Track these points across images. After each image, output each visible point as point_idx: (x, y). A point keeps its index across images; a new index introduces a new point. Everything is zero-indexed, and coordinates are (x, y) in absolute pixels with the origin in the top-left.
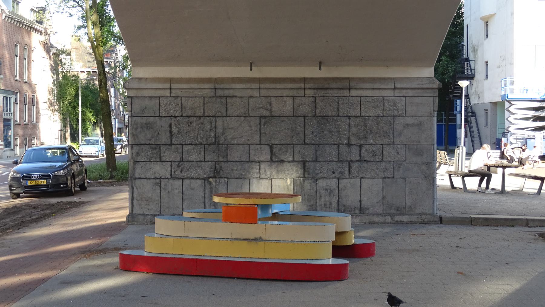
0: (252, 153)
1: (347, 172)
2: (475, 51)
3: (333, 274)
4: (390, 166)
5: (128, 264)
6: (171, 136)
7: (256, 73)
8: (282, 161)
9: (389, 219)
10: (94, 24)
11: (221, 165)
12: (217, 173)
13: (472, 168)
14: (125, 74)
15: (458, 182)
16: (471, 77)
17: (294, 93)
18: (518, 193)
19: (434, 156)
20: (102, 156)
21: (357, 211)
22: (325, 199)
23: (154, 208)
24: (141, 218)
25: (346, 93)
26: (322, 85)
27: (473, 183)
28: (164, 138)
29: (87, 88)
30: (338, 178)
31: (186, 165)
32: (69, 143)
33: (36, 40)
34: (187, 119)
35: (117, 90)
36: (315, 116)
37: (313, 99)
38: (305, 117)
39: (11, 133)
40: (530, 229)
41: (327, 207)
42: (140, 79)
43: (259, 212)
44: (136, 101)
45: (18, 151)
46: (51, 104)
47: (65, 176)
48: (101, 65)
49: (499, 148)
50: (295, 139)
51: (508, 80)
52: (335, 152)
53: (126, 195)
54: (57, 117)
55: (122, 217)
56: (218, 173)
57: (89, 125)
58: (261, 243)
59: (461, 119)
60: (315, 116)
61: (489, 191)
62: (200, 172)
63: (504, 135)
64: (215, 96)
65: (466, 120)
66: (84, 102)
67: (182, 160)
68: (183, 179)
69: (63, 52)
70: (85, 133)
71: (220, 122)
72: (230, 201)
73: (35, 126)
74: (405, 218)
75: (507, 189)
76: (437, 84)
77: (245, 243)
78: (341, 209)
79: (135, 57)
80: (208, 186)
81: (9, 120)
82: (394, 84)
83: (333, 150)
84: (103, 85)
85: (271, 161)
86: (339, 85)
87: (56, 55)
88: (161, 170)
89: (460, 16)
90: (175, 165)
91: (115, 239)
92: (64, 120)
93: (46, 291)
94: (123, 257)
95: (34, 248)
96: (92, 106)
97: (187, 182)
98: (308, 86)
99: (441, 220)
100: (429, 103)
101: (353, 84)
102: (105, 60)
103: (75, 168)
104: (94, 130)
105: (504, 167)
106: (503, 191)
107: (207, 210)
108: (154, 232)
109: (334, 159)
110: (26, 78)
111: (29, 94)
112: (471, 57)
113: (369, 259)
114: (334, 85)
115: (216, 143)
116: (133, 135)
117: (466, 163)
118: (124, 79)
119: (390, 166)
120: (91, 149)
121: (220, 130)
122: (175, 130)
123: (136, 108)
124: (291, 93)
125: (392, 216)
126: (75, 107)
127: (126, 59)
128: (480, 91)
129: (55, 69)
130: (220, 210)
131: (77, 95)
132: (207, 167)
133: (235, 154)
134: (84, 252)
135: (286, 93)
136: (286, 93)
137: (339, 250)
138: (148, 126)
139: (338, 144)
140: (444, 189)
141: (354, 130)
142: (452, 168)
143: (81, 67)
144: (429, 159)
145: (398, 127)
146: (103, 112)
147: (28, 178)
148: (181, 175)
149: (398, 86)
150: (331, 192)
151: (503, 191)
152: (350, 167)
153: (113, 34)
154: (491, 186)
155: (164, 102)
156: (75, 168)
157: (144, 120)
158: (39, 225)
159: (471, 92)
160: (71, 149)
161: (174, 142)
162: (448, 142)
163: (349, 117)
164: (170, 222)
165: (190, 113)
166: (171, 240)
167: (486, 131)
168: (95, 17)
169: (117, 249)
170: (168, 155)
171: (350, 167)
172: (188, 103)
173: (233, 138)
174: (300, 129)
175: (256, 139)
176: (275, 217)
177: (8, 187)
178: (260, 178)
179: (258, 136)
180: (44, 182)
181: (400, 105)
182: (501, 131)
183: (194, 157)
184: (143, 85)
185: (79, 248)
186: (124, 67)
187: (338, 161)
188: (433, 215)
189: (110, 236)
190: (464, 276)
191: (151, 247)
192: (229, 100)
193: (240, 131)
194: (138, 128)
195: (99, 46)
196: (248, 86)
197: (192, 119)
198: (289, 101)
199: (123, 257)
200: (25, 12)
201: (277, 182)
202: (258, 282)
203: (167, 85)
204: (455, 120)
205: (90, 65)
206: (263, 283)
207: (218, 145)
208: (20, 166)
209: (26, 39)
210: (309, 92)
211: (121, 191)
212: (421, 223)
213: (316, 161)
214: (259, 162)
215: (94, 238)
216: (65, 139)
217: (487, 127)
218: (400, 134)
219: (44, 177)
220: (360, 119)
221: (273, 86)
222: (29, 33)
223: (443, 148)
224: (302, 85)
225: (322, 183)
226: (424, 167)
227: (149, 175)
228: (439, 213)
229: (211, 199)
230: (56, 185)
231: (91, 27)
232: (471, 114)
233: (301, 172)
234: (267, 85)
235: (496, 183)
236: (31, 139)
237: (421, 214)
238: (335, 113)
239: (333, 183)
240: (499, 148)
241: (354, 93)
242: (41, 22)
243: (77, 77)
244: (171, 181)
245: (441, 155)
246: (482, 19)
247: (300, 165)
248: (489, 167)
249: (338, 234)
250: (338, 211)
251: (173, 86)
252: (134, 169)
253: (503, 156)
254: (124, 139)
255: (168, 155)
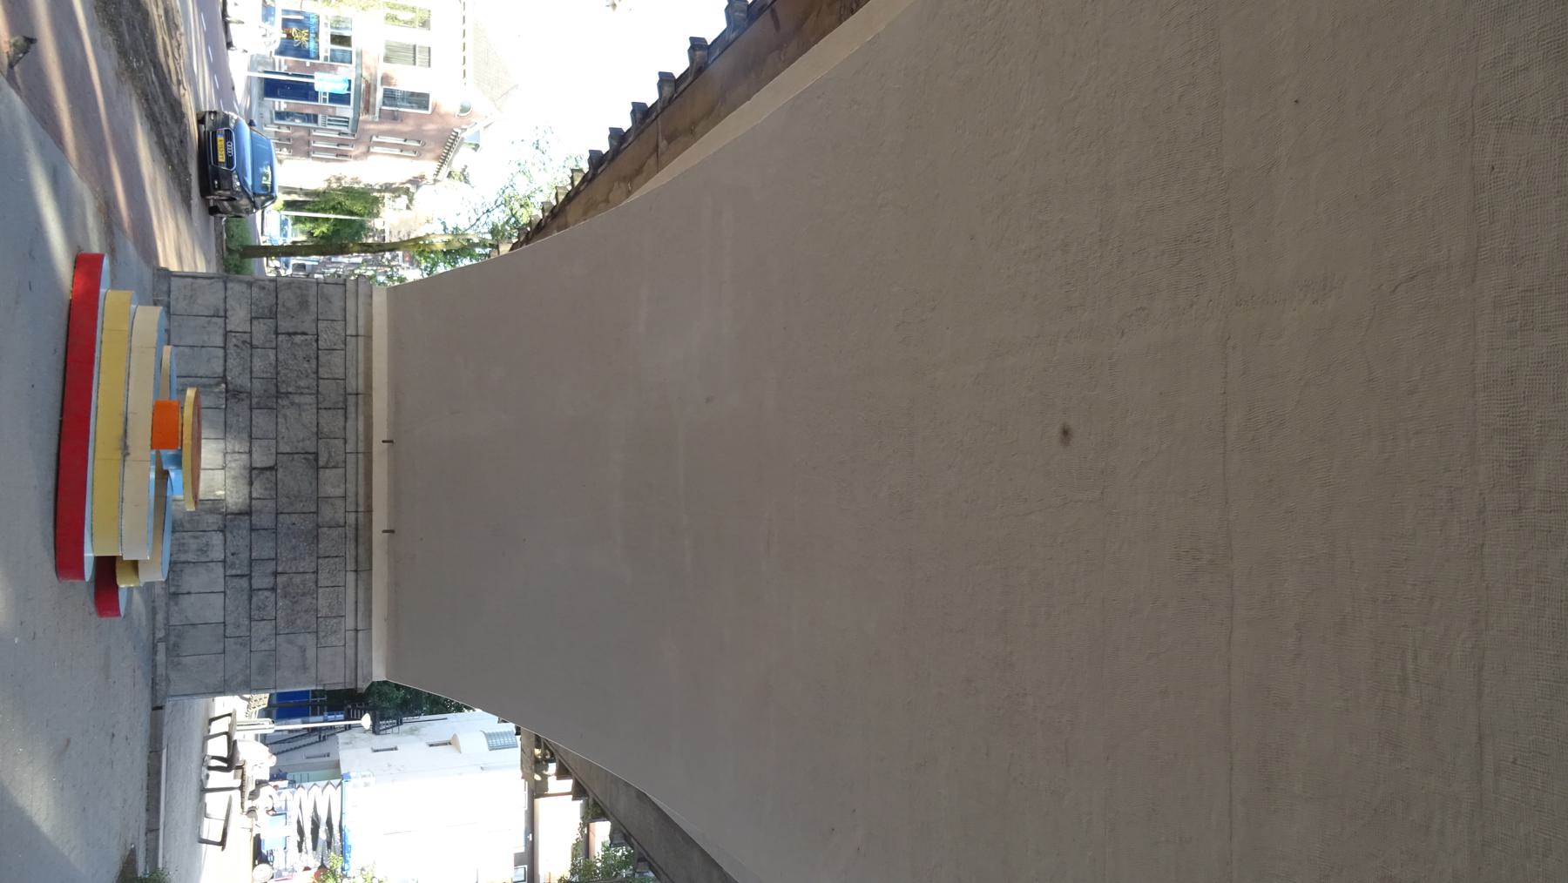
0: (264, 443)
2: (412, 732)
3: (67, 556)
4: (243, 632)
5: (86, 265)
6: (289, 334)
7: (378, 448)
8: (251, 484)
9: (160, 634)
10: (447, 243)
11: (240, 402)
12: (233, 394)
13: (239, 745)
14: (381, 279)
15: (217, 727)
16: (375, 730)
17: (351, 499)
18: (201, 812)
19: (258, 690)
20: (264, 241)
21: (172, 590)
22: (193, 544)
23: (179, 305)
24: (165, 288)
25: (351, 566)
26: (361, 535)
27: (218, 747)
28: (285, 325)
29: (362, 228)
30: (224, 561)
31: (246, 353)
32: (281, 198)
33: (427, 166)
34: (313, 356)
35: (358, 265)
36: (318, 526)
37: (342, 522)
38: (317, 513)
39: (298, 122)
40: (142, 838)
41: (179, 547)
42: (371, 296)
43: (171, 452)
44: (340, 290)
45: (272, 129)
46: (339, 179)
47: (231, 188)
48: (393, 247)
49: (272, 778)
50: (285, 500)
51: (371, 780)
52: (265, 555)
53: (202, 268)
54: (320, 185)
55: (166, 261)
56: (234, 396)
57: (309, 226)
58: (119, 455)
59: (316, 723)
60: (318, 526)
61: (205, 771)
62: (236, 372)
63: (292, 783)
64: (346, 394)
65: (314, 729)
66: (342, 223)
67: (252, 347)
68: (224, 348)
69: (411, 200)
70: (297, 220)
71: (310, 399)
72: (188, 412)
73: (308, 155)
74: (161, 657)
75: (208, 796)
76: (363, 686)
77: (121, 432)
78: (175, 567)
79: (402, 293)
80: (212, 381)
81: (316, 121)
82: (362, 630)
83: (268, 552)
84: (367, 248)
85: (252, 469)
86: (362, 557)
87: (407, 192)
88: (239, 318)
89: (459, 709)
90: (247, 337)
91: (130, 250)
92: (316, 193)
93: (41, 146)
94: (98, 259)
95: (114, 134)
96: (336, 233)
97: (221, 353)
99: (157, 708)
100: (336, 679)
101: (363, 575)
102: (400, 253)
103: (244, 202)
104: (303, 232)
105: (241, 788)
106: (204, 790)
107: (175, 380)
108: (140, 303)
110: (375, 149)
111: (354, 151)
112: (402, 728)
113: (93, 609)
114: (361, 549)
115: (278, 395)
116: (291, 283)
117: (251, 735)
118: (374, 277)
119: (243, 632)
120: (272, 225)
121: (297, 399)
122: (298, 339)
123: (330, 290)
124: (351, 494)
125: (165, 639)
126: (334, 209)
127: (401, 279)
128: (358, 746)
129: (387, 188)
130: (175, 398)
131: (351, 213)
132: (243, 381)
133: (261, 420)
134: (107, 203)
135: (351, 487)
136: (351, 487)
137: (107, 568)
138: (304, 304)
139: (275, 559)
140: (208, 709)
141: (297, 579)
142: (240, 717)
143: (391, 221)
144: (254, 685)
145: (300, 639)
146: (331, 244)
147: (228, 136)
148: (230, 345)
149: (360, 635)
150: (202, 551)
151: (204, 790)
152: (242, 576)
153: (435, 265)
154: (212, 773)
155: (339, 326)
156: (244, 202)
157: (312, 299)
158: (155, 148)
159: (354, 732)
160: (273, 199)
161: (281, 338)
162: (282, 708)
163: (316, 572)
164: (155, 328)
165: (323, 359)
166: (126, 327)
167: (298, 757)
168: (457, 245)
169: (113, 251)
170: (261, 330)
171: (242, 576)
172: (337, 358)
173: (285, 417)
174: (299, 506)
176: (163, 476)
177: (215, 108)
178: (225, 454)
179: (288, 449)
180: (222, 158)
181: (332, 639)
182: (297, 777)
183: (258, 364)
184: (361, 299)
185: (115, 197)
186: (390, 278)
187: (251, 560)
188: (167, 695)
189: (136, 243)
190: (61, 754)
191: (112, 300)
192: (341, 412)
193: (296, 426)
194: (302, 291)
195: (417, 247)
196: (361, 437)
197: (314, 362)
198: (339, 492)
199: (98, 259)
200: (460, 158)
201: (218, 472)
202: (54, 450)
203: (361, 332)
204: (314, 714)
205: (395, 233)
206: (53, 458)
207: (275, 396)
208: (246, 130)
209: (429, 155)
210: (351, 518)
211: (208, 262)
212: (154, 682)
214: (250, 452)
215: (132, 220)
216: (289, 193)
217: (299, 758)
218: (290, 642)
219: (229, 160)
221: (361, 471)
222: (438, 158)
223: (275, 701)
224: (361, 509)
225: (217, 539)
226: (241, 678)
227: (230, 302)
228: (169, 705)
229: (192, 386)
230: (217, 174)
231: (446, 238)
232: (322, 735)
233: (234, 509)
234: (361, 464)
235: (216, 779)
236: (288, 147)
237: (168, 679)
238: (321, 553)
239: (218, 554)
240: (272, 778)
241: (351, 577)
242: (450, 175)
243: (377, 215)
244: (221, 331)
245: (262, 700)
246: (455, 737)
247: (245, 508)
248: (241, 767)
249: (134, 565)
250: (173, 564)
251: (361, 340)
252: (240, 282)
253: (260, 783)
254: (289, 272)
255: (261, 330)
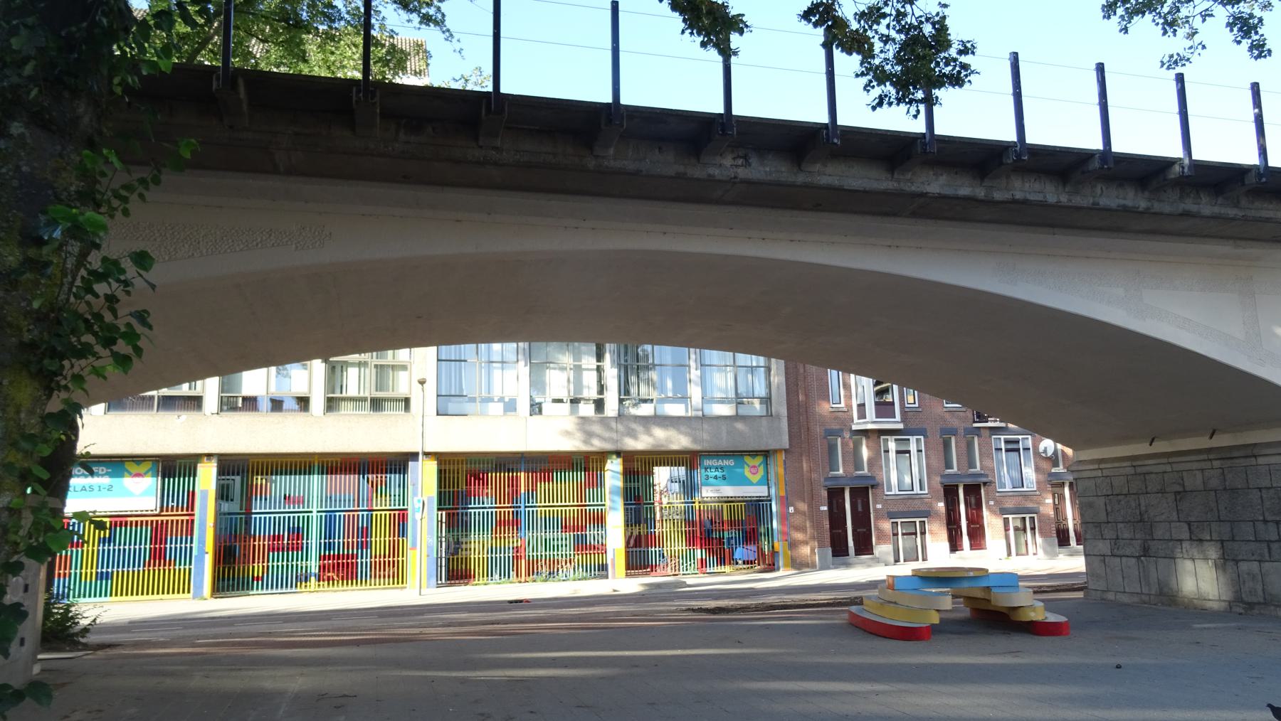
1: (1267, 555)
12: (1146, 552)
17: (1203, 465)
36: (1225, 489)
44: (1080, 482)
60: (1225, 489)
97: (1124, 559)
98: (1211, 457)
101: (1256, 452)
109: (1251, 538)
114: (1236, 454)
121: (1143, 508)
133: (1159, 533)
135: (1195, 466)
136: (1195, 466)
141: (1267, 504)
150: (1254, 577)
163: (1260, 489)
175: (1175, 518)
183: (1126, 535)
198: (1199, 475)
207: (1142, 522)
210: (1217, 464)
213: (1233, 540)
220: (1272, 491)
241: (1261, 460)
247: (1219, 545)
255: (1108, 533)
